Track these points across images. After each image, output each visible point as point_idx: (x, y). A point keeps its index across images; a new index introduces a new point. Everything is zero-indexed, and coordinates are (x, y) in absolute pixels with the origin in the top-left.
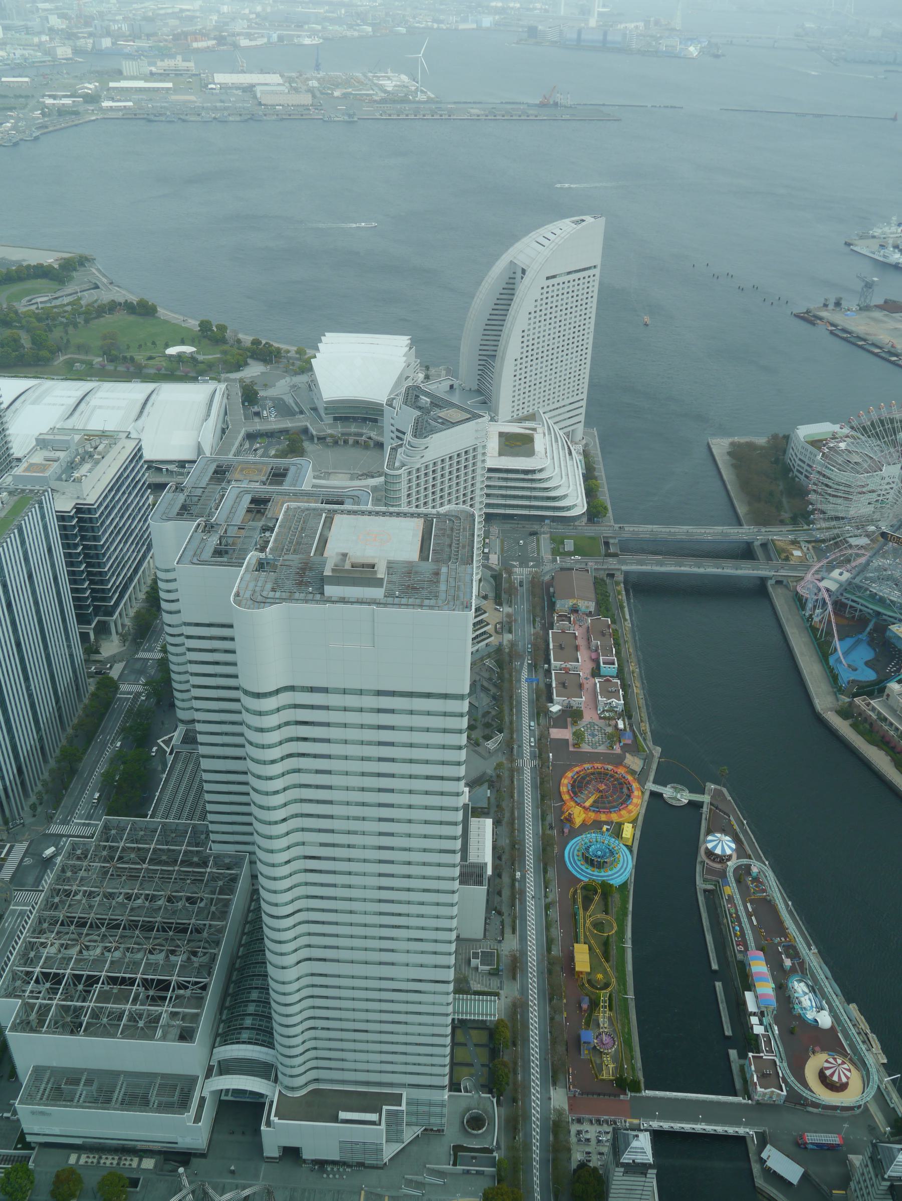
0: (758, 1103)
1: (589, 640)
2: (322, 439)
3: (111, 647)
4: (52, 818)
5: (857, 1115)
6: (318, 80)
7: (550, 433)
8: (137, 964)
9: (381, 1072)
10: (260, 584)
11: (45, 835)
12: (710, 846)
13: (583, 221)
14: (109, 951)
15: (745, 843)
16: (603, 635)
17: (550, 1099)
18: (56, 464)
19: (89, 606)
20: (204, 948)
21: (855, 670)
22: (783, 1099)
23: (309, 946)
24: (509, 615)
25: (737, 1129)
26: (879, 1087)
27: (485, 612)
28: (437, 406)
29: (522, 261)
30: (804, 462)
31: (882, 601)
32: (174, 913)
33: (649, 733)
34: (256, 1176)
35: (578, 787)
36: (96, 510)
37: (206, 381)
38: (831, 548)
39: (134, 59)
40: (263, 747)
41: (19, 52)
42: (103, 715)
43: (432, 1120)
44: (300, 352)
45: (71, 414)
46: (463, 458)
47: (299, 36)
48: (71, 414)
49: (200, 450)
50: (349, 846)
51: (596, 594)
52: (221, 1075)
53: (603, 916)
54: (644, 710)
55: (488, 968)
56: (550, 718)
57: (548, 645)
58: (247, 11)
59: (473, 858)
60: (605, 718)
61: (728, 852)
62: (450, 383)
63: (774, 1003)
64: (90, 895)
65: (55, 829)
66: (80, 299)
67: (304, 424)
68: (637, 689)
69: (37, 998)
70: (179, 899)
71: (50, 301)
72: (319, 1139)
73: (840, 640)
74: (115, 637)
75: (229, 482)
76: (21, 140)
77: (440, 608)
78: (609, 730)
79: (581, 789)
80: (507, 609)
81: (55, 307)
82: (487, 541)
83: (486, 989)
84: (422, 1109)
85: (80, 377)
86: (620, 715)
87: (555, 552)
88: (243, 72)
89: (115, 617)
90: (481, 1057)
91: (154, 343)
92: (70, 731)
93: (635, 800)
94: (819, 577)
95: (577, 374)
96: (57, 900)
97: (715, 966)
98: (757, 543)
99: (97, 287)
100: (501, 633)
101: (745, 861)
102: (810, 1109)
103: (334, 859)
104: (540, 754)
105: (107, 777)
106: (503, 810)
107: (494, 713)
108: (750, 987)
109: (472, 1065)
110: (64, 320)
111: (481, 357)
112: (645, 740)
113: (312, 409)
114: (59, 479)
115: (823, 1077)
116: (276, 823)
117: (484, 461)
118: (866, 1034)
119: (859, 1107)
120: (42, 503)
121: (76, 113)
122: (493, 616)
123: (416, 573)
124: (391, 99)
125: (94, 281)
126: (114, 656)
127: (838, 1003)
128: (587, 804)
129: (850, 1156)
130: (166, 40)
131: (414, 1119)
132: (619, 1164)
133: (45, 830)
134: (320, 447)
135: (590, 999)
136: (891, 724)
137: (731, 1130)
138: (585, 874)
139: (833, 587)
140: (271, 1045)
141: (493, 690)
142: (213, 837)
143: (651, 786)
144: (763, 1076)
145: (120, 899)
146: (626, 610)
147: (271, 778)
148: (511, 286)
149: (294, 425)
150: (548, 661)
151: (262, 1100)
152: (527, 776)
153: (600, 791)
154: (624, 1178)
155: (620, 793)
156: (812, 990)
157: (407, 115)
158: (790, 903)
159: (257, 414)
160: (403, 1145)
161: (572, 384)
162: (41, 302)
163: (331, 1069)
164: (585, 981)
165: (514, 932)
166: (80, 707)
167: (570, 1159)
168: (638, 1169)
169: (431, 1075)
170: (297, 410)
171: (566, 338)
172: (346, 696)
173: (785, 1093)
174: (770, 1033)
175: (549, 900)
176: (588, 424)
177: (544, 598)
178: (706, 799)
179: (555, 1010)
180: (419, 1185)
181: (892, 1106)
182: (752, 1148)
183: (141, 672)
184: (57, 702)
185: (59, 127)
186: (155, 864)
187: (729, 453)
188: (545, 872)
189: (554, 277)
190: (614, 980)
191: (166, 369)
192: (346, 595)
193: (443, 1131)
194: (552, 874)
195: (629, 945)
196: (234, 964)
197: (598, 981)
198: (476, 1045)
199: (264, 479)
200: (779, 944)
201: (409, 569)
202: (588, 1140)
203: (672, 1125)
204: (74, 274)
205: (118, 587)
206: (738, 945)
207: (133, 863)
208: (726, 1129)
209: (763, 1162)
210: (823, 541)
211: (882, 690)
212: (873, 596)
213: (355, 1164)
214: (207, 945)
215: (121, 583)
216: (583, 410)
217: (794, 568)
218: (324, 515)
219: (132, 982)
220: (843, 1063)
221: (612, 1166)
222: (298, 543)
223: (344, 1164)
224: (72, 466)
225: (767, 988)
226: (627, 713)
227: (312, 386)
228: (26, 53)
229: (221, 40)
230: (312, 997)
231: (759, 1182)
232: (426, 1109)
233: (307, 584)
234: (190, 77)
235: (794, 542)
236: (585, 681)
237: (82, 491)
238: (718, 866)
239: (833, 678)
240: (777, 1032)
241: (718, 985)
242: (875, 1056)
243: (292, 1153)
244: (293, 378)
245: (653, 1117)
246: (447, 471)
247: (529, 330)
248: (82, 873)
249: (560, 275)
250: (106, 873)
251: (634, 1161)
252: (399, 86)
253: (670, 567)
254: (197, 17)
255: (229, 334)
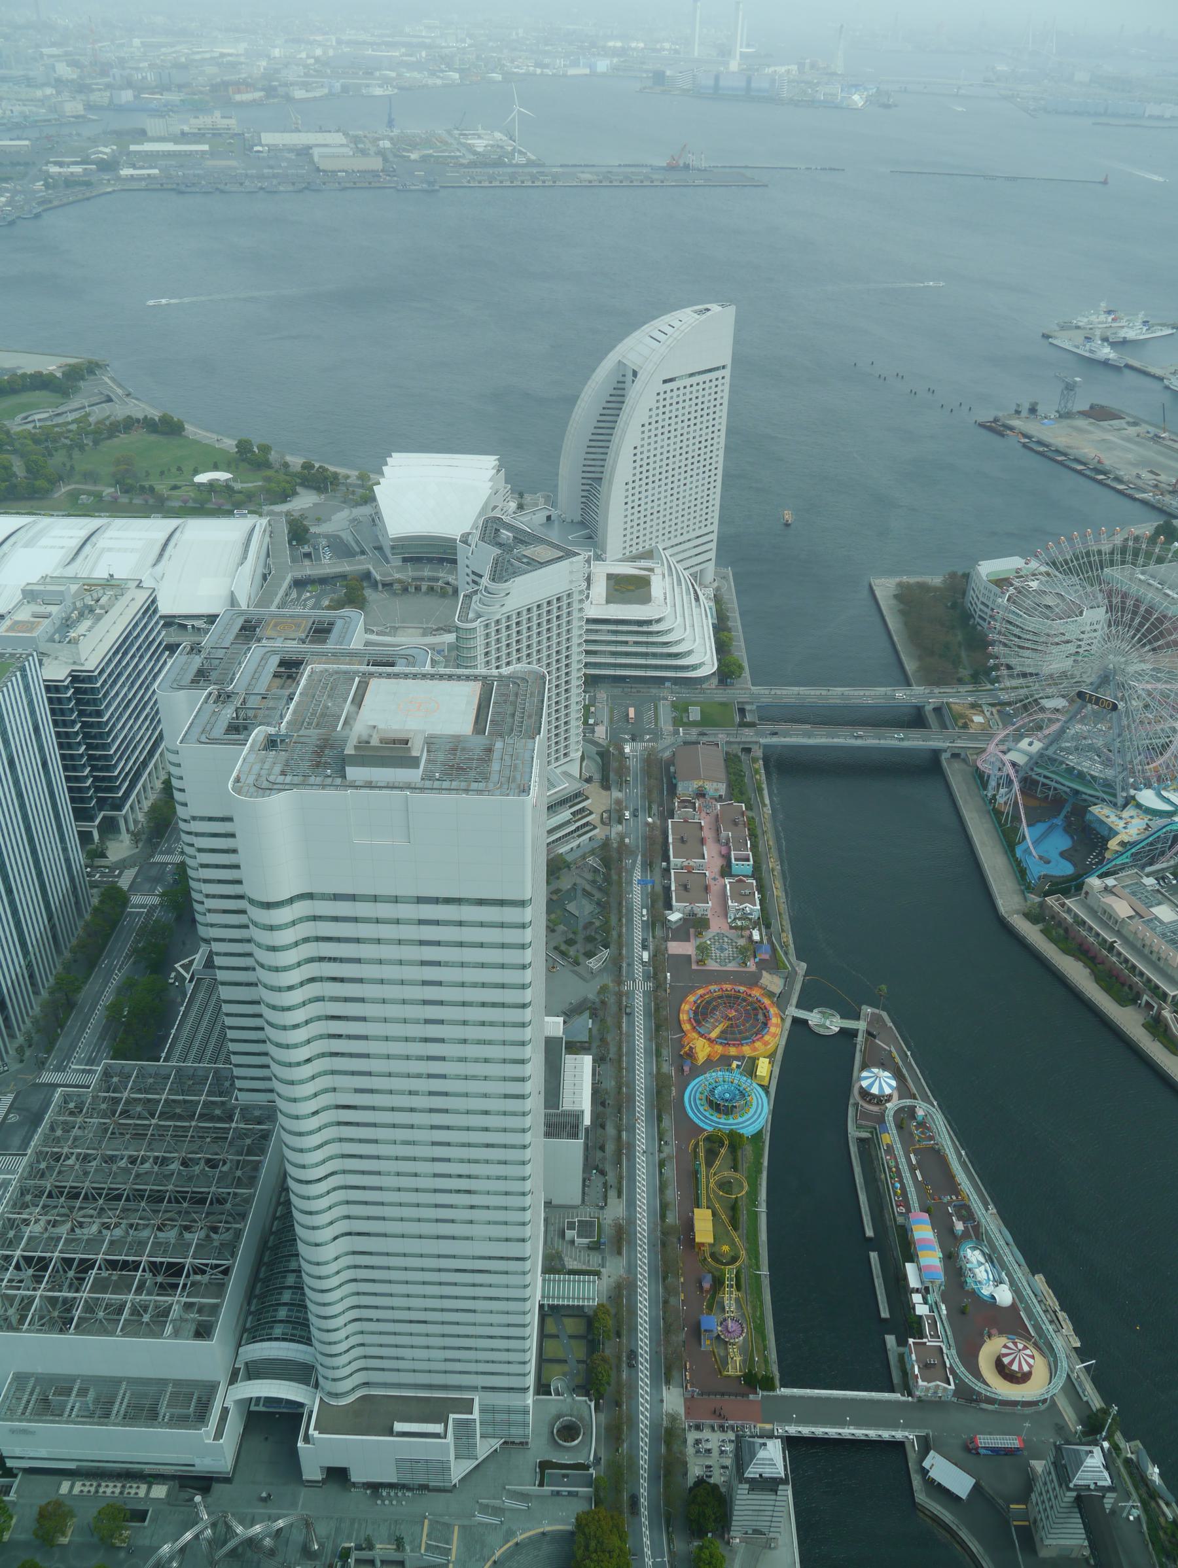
0: (920, 1400)
1: (718, 831)
2: (387, 585)
3: (120, 848)
4: (43, 1063)
5: (1044, 1409)
6: (391, 139)
7: (671, 574)
8: (142, 1244)
9: (445, 1372)
10: (266, 766)
11: (35, 1085)
12: (864, 1084)
13: (708, 310)
14: (108, 1228)
15: (909, 1080)
16: (736, 824)
17: (662, 1401)
18: (47, 621)
19: (91, 798)
20: (226, 1222)
21: (1048, 862)
22: (951, 1393)
23: (348, 1217)
24: (618, 802)
25: (893, 1433)
26: (1068, 1375)
27: (587, 798)
28: (522, 542)
29: (632, 360)
30: (987, 606)
31: (1081, 776)
32: (190, 1179)
33: (792, 946)
34: (294, 1505)
35: (702, 1014)
36: (96, 679)
37: (243, 516)
38: (1022, 712)
39: (163, 117)
40: (277, 969)
41: (17, 109)
42: (109, 936)
43: (514, 1431)
44: (363, 477)
45: (73, 559)
46: (555, 605)
47: (368, 86)
48: (73, 559)
49: (233, 601)
50: (410, 1093)
51: (728, 773)
52: (250, 1379)
53: (732, 1173)
54: (786, 917)
55: (587, 1241)
56: (668, 929)
57: (667, 837)
58: (303, 55)
59: (567, 1104)
60: (736, 928)
61: (888, 1091)
62: (548, 513)
63: (940, 1277)
64: (86, 1158)
65: (47, 1077)
66: (88, 415)
67: (365, 567)
68: (778, 890)
69: (19, 1288)
70: (196, 1162)
71: (50, 418)
72: (370, 1456)
73: (1029, 825)
74: (126, 838)
75: (259, 640)
76: (19, 217)
77: (490, 792)
78: (742, 942)
79: (705, 1016)
80: (616, 794)
81: (57, 425)
82: (592, 709)
83: (584, 1267)
84: (499, 1417)
85: (86, 512)
86: (756, 924)
87: (677, 722)
88: (297, 130)
89: (124, 812)
90: (578, 1351)
91: (179, 469)
92: (67, 954)
93: (773, 1029)
94: (1004, 748)
95: (704, 500)
96: (43, 1165)
97: (869, 1233)
98: (929, 708)
99: (109, 400)
100: (609, 824)
101: (908, 1102)
102: (984, 1406)
103: (373, 1108)
104: (655, 974)
105: (114, 1010)
106: (608, 1044)
107: (598, 924)
108: (911, 1257)
109: (565, 1361)
110: (67, 442)
111: (584, 481)
112: (786, 954)
113: (375, 548)
114: (51, 640)
115: (1001, 1368)
116: (298, 1064)
117: (581, 610)
118: (1055, 1312)
119: (1045, 1401)
120: (25, 670)
121: (88, 184)
122: (598, 801)
123: (463, 749)
124: (482, 162)
125: (107, 392)
126: (124, 860)
127: (1020, 1275)
128: (713, 1035)
129: (1033, 1462)
130: (201, 93)
131: (490, 1430)
132: (742, 1479)
133: (35, 1079)
134: (385, 595)
135: (714, 1277)
136: (1091, 929)
137: (886, 1435)
138: (710, 1122)
139: (1021, 760)
140: (308, 1341)
141: (598, 895)
142: (239, 1084)
143: (793, 1011)
144: (926, 1367)
145: (123, 1163)
146: (766, 792)
147: (289, 1009)
148: (619, 392)
149: (352, 568)
150: (666, 858)
151: (300, 1410)
152: (639, 1002)
153: (730, 1019)
154: (750, 1497)
155: (753, 1020)
156: (989, 1259)
157: (480, 182)
158: (963, 1153)
159: (308, 555)
160: (477, 1462)
161: (699, 513)
162: (40, 420)
163: (383, 1370)
164: (707, 1255)
165: (619, 1196)
166: (80, 924)
167: (686, 1474)
168: (769, 1485)
169: (508, 1374)
170: (358, 550)
171: (689, 456)
172: (378, 904)
173: (952, 1387)
174: (936, 1314)
175: (663, 1155)
176: (721, 560)
177: (663, 780)
178: (861, 1025)
179: (669, 1291)
180: (497, 1511)
181: (1085, 1399)
182: (912, 1457)
183: (157, 880)
184: (50, 919)
185: (65, 200)
186: (205, 1121)
187: (896, 596)
188: (660, 1119)
189: (671, 380)
190: (743, 1253)
191: (195, 501)
192: (374, 779)
193: (527, 1443)
194: (667, 1122)
195: (763, 1208)
196: (266, 1242)
197: (723, 1255)
198: (571, 1337)
199: (303, 636)
200: (949, 1203)
201: (456, 744)
202: (709, 1451)
203: (813, 1429)
204: (82, 384)
205: (127, 774)
206: (898, 1206)
207: (139, 1118)
208: (880, 1433)
209: (924, 1472)
210: (1009, 704)
211: (1079, 887)
212: (1070, 770)
213: (419, 1486)
214: (230, 1219)
215: (131, 768)
216: (713, 545)
217: (973, 737)
218: (357, 679)
219: (136, 1266)
220: (1025, 1348)
221: (735, 1482)
222: (323, 715)
223: (404, 1487)
224: (67, 624)
225: (932, 1258)
226: (765, 921)
227: (376, 519)
228: (26, 109)
229: (270, 91)
230: (355, 1280)
231: (921, 1497)
232: (505, 1416)
233: (326, 765)
234: (231, 138)
235: (974, 706)
236: (712, 883)
237: (78, 654)
238: (875, 1109)
239: (1021, 872)
240: (945, 1312)
241: (874, 1256)
242: (1065, 1339)
243: (338, 1475)
244: (354, 510)
245: (790, 1421)
246: (535, 622)
247: (642, 446)
248: (76, 1132)
249: (680, 377)
250: (106, 1130)
251: (761, 1475)
252: (492, 146)
253: (820, 739)
254: (241, 63)
255: (273, 456)
